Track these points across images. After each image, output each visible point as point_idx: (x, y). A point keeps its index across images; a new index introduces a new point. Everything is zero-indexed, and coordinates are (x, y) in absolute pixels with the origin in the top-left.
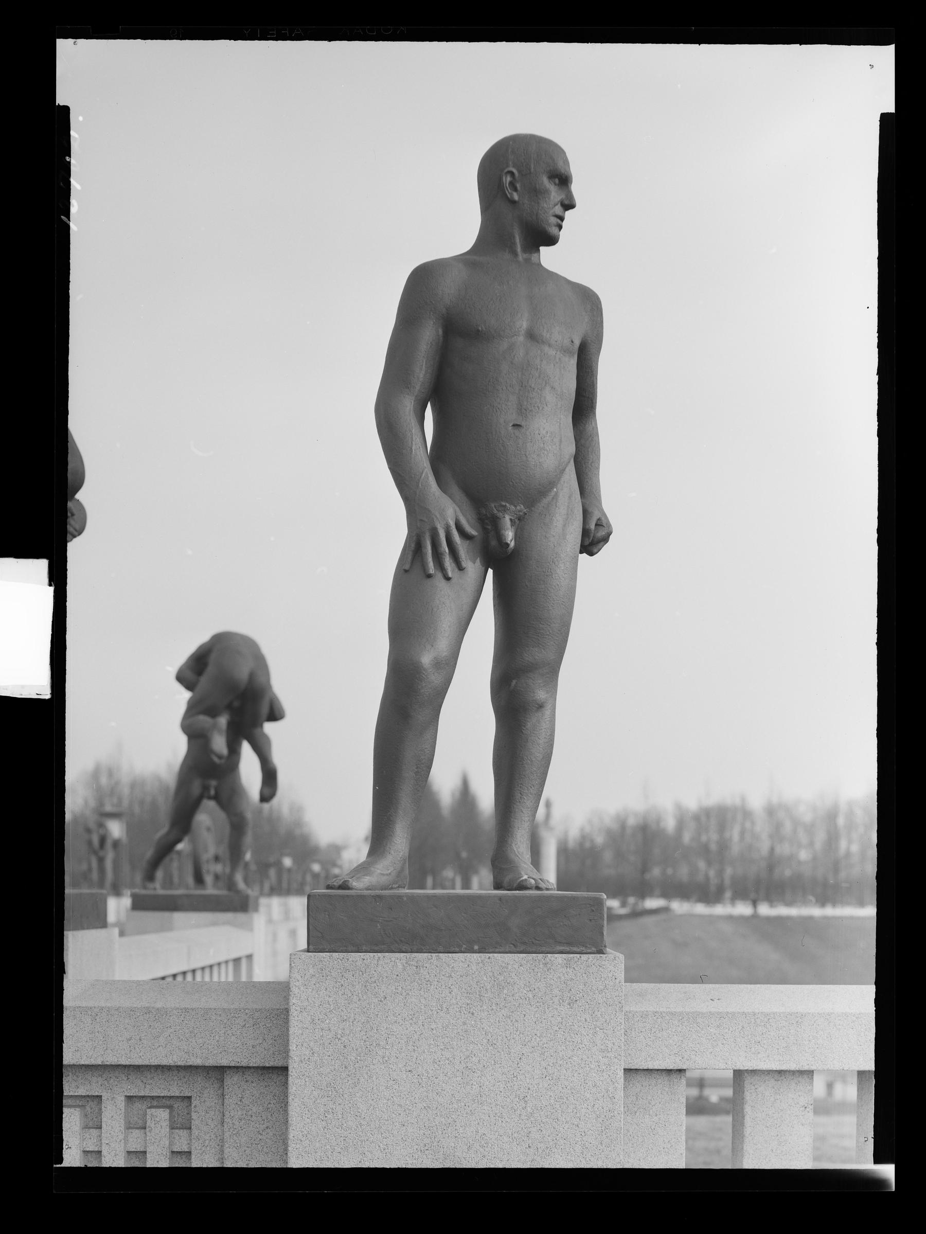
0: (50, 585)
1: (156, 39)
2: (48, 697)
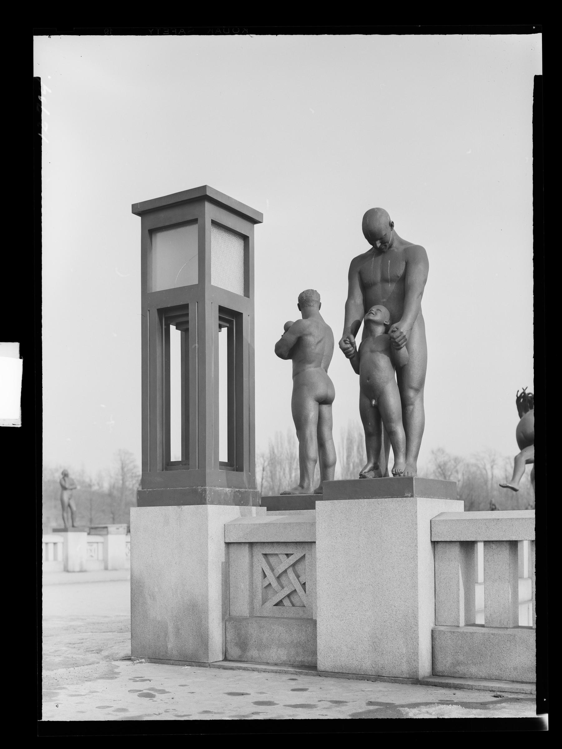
0: (21, 358)
1: (535, 311)
2: (20, 426)
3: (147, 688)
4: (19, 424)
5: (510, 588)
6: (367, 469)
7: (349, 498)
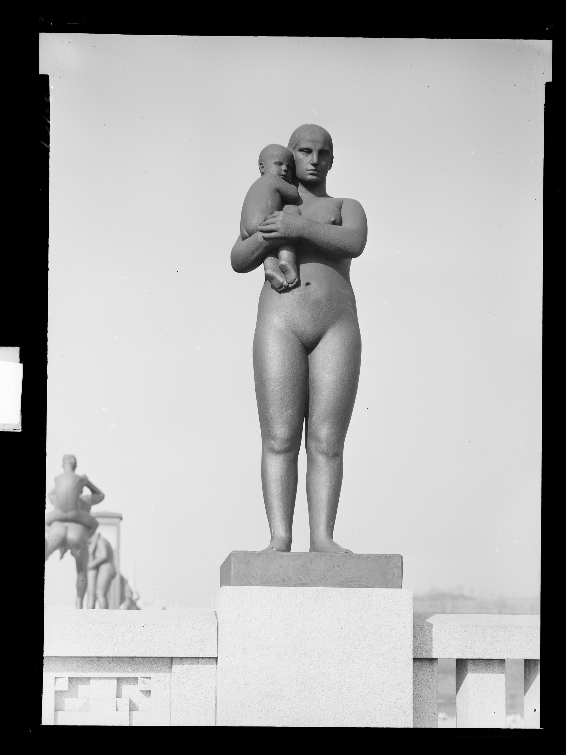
0: (21, 362)
2: (20, 431)
4: (19, 429)
5: (272, 180)
6: (322, 513)
7: (233, 263)
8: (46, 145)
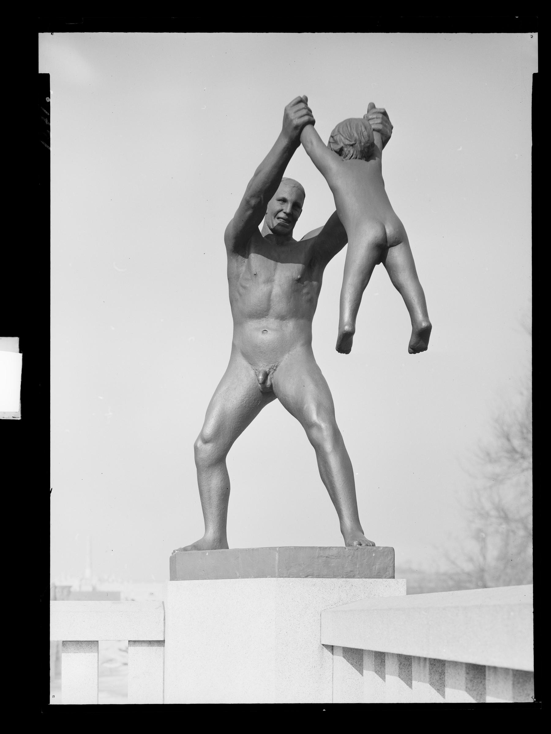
0: (20, 352)
2: (20, 419)
3: (177, 549)
4: (18, 417)
8: (48, 147)
